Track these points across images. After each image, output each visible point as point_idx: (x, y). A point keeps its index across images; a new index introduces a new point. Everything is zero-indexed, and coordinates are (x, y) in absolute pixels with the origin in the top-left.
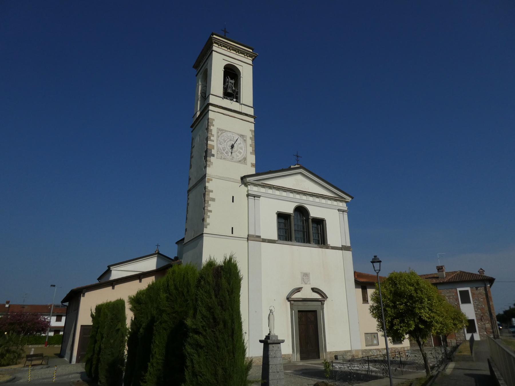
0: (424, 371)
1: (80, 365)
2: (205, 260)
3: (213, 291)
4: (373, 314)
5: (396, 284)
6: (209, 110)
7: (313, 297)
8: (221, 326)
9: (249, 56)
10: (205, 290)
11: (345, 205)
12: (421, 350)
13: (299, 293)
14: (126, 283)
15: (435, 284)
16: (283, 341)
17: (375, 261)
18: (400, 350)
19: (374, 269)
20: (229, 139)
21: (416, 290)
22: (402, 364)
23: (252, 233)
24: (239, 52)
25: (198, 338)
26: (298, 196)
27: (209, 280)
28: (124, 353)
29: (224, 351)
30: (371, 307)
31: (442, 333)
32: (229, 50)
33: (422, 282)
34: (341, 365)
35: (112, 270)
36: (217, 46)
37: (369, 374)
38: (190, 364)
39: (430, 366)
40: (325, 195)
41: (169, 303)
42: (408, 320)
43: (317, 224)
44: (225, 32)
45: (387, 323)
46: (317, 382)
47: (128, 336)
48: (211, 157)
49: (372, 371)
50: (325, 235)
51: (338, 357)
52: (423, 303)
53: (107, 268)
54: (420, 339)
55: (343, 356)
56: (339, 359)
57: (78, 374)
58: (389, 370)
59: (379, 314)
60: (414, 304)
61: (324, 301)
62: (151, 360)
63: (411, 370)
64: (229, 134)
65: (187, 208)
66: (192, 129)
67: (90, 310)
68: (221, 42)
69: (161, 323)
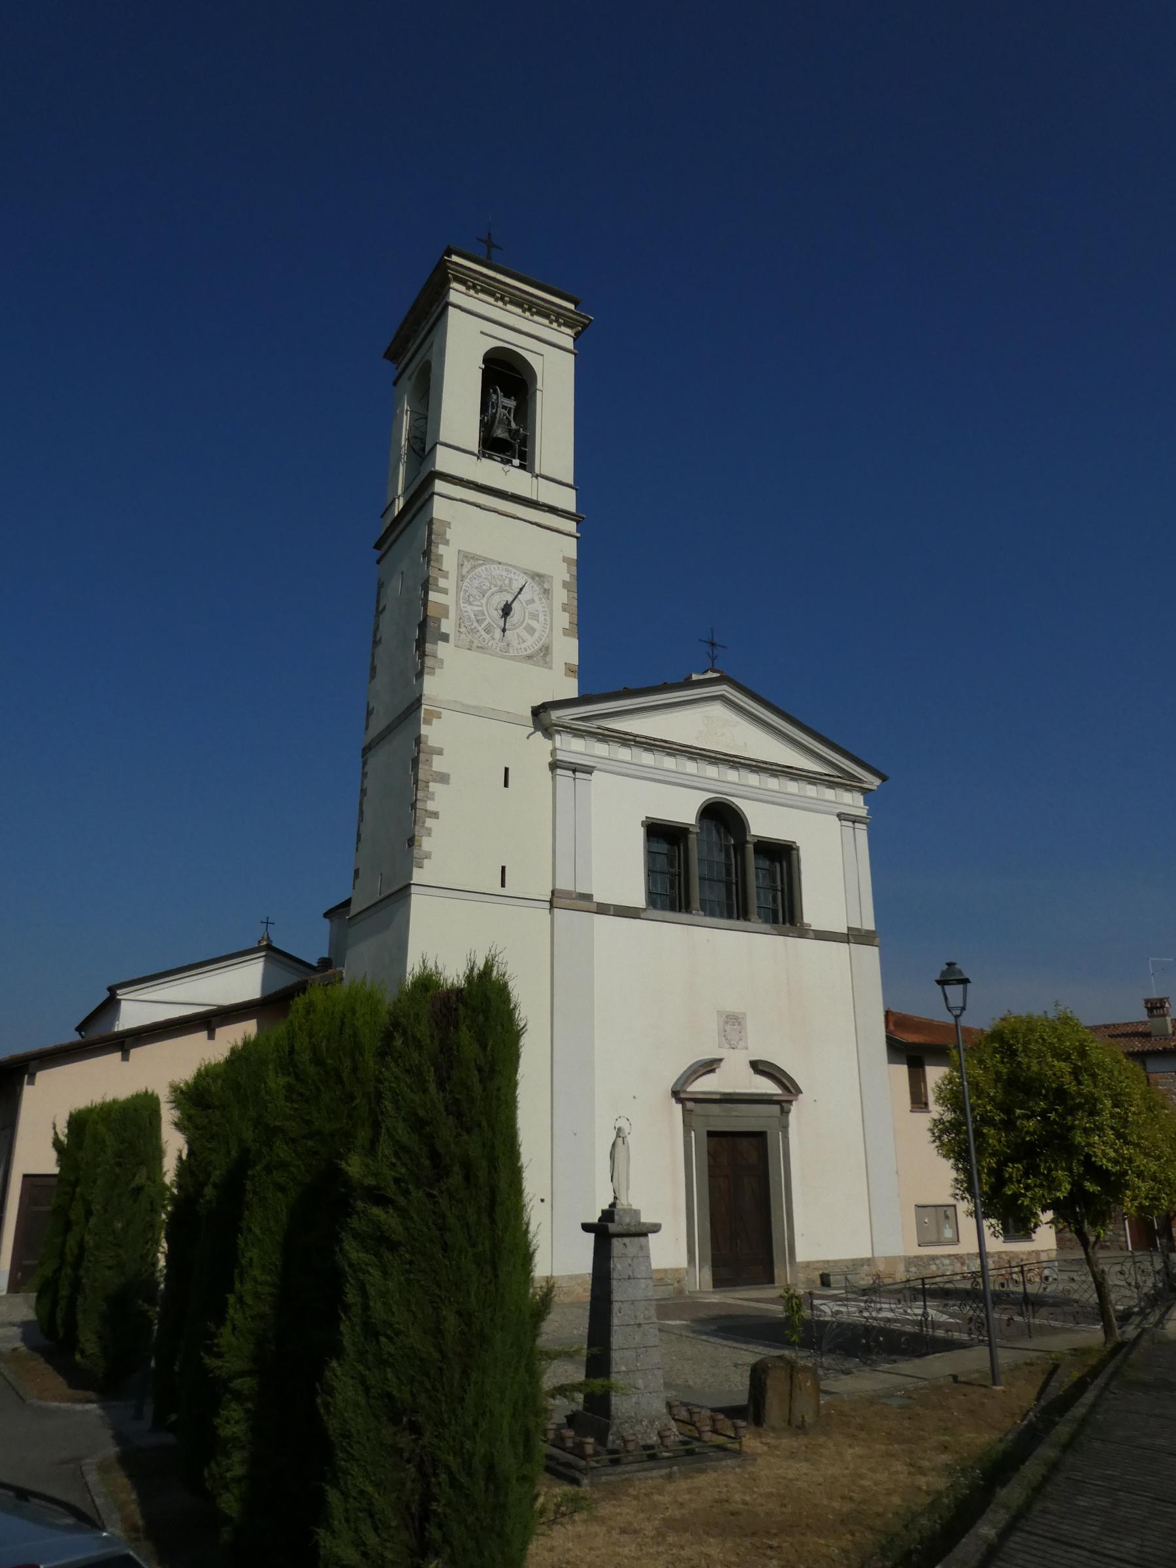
0: (1099, 1327)
1: (19, 1298)
2: (413, 966)
3: (432, 1069)
4: (942, 1145)
5: (1013, 1053)
6: (433, 494)
7: (757, 1088)
8: (456, 1178)
9: (566, 325)
10: (408, 1067)
11: (859, 799)
12: (1089, 1260)
13: (711, 1075)
14: (184, 1037)
15: (1140, 1057)
16: (656, 1228)
17: (950, 977)
18: (1026, 1260)
19: (947, 1004)
20: (495, 586)
21: (1076, 1073)
22: (1030, 1302)
23: (564, 884)
24: (534, 310)
25: (383, 1216)
26: (712, 771)
27: (419, 1035)
28: (154, 1264)
29: (463, 1257)
30: (936, 1122)
31: (1156, 1208)
32: (500, 304)
33: (1097, 1048)
34: (839, 1305)
35: (120, 1000)
36: (462, 288)
37: (925, 1332)
38: (359, 1299)
39: (1116, 1311)
40: (796, 769)
41: (296, 1106)
42: (1050, 1165)
43: (772, 861)
44: (490, 244)
45: (984, 1176)
46: (762, 1357)
47: (169, 1208)
48: (440, 642)
49: (935, 1325)
50: (796, 894)
51: (831, 1277)
52: (1099, 1114)
53: (107, 994)
54: (1086, 1226)
55: (845, 1275)
56: (832, 1286)
57: (15, 1328)
58: (988, 1322)
59: (958, 1147)
60: (1069, 1118)
61: (790, 1102)
62: (237, 1285)
63: (1057, 1324)
64: (497, 571)
65: (361, 804)
66: (378, 553)
67: (52, 1126)
68: (477, 276)
69: (268, 1169)
